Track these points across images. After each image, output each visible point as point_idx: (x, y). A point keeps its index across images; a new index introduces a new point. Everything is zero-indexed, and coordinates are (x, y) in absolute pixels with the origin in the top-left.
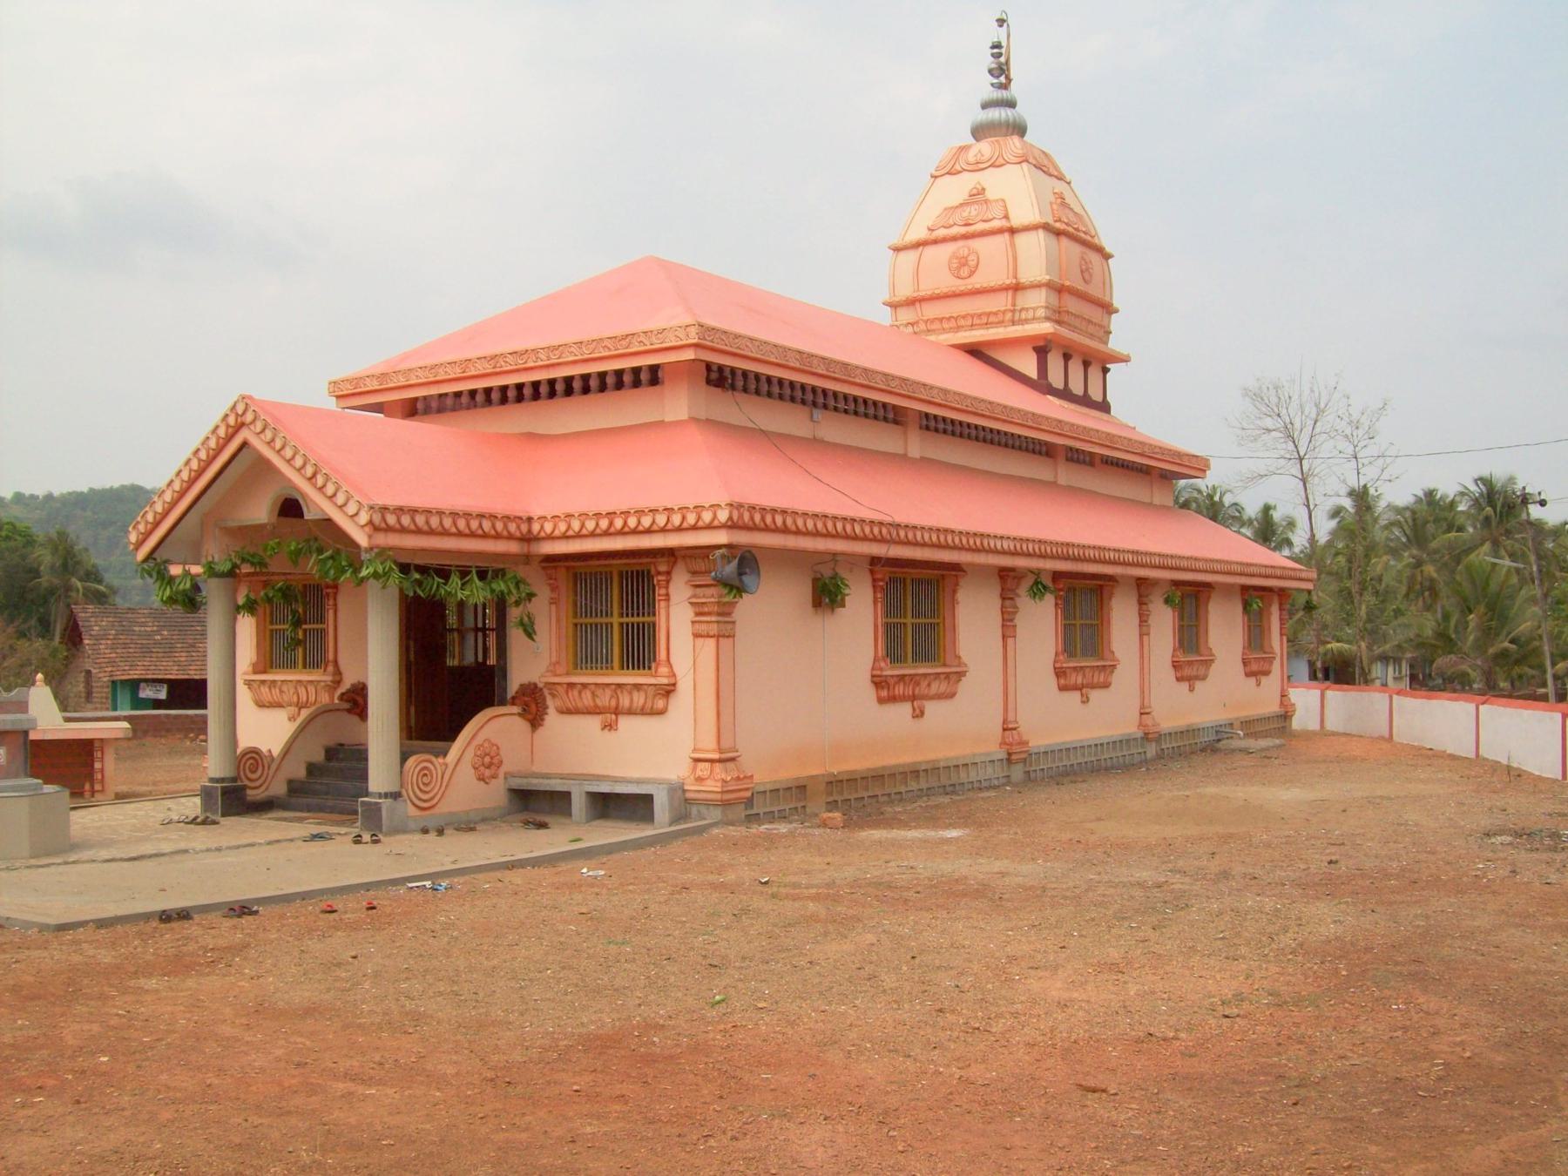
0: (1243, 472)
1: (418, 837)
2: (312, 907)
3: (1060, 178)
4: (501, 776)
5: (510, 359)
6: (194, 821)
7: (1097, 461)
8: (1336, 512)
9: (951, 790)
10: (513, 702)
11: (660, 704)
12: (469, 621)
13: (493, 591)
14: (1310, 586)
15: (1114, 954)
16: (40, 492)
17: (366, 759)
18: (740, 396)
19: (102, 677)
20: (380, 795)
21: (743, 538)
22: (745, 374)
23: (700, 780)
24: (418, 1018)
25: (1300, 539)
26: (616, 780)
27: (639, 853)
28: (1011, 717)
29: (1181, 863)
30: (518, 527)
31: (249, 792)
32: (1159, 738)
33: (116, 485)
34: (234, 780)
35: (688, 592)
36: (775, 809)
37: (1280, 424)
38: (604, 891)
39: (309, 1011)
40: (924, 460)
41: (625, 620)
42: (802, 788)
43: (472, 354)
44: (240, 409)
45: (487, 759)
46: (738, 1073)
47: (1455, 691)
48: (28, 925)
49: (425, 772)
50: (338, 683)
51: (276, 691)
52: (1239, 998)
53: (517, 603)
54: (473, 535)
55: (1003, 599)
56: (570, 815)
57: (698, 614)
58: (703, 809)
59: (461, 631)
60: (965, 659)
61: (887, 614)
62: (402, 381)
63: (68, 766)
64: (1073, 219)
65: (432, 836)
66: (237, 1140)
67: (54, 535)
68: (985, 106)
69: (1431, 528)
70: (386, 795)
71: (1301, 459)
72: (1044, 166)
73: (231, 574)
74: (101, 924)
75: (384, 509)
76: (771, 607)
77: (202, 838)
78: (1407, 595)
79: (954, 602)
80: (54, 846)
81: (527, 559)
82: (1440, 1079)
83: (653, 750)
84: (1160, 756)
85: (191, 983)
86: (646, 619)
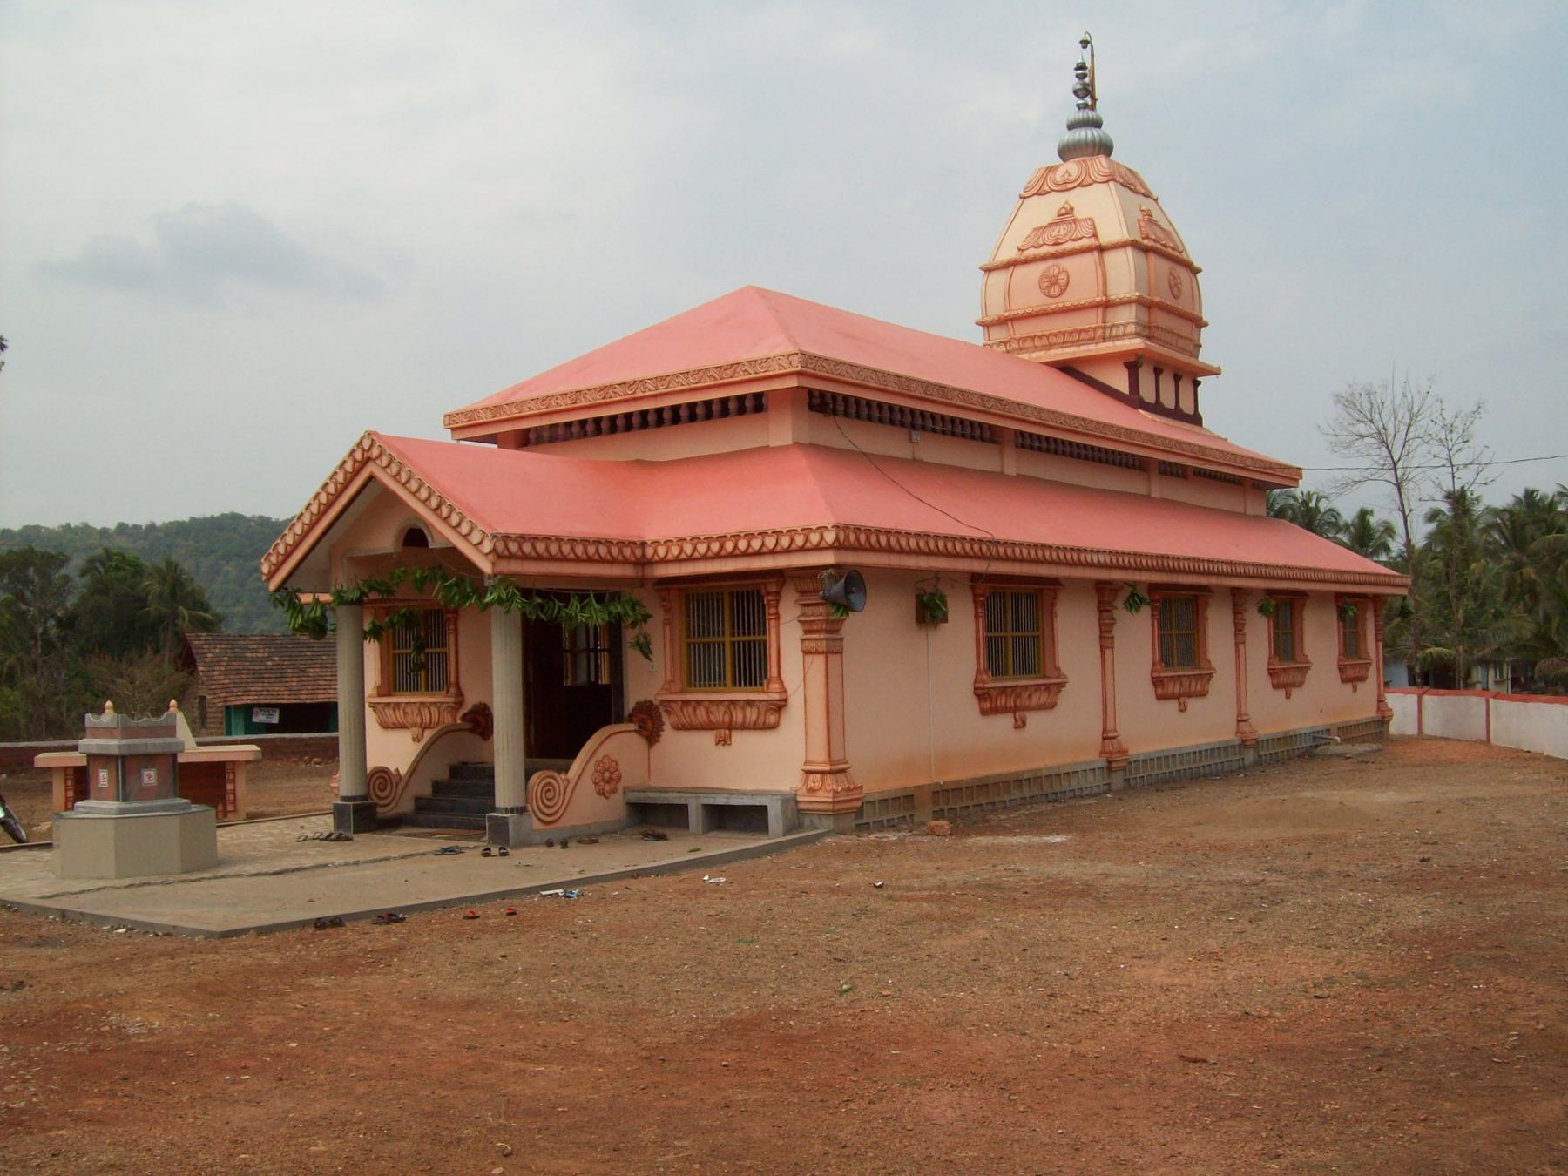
0: (1336, 476)
1: (543, 849)
2: (456, 915)
3: (1147, 195)
4: (620, 789)
5: (619, 390)
6: (328, 838)
7: (1190, 473)
8: (1433, 516)
9: (1053, 798)
10: (630, 719)
11: (772, 719)
12: (582, 643)
13: (610, 613)
14: (1404, 592)
15: (1213, 945)
16: (143, 521)
17: (493, 777)
18: (841, 420)
19: (216, 702)
20: (506, 810)
21: (850, 558)
22: (846, 398)
23: (812, 791)
24: (571, 1008)
25: (1397, 545)
26: (730, 793)
27: (756, 861)
28: (1110, 726)
29: (1278, 862)
30: (633, 552)
31: (379, 810)
32: (1257, 744)
33: (217, 514)
34: (365, 798)
35: (797, 611)
36: (884, 818)
37: (1373, 430)
38: (728, 896)
39: (471, 1004)
40: (1021, 478)
41: (736, 639)
42: (909, 798)
43: (582, 386)
44: (366, 444)
45: (607, 775)
46: (870, 1050)
47: (1556, 694)
48: (195, 932)
49: (548, 788)
50: (460, 703)
51: (400, 714)
52: (1330, 981)
53: (634, 625)
54: (590, 560)
55: (1101, 611)
56: (687, 826)
57: (807, 632)
58: (816, 820)
59: (574, 652)
60: (1064, 671)
61: (988, 628)
62: (515, 413)
63: (205, 784)
64: (1160, 235)
65: (557, 849)
66: (429, 1108)
67: (163, 565)
68: (1072, 126)
69: (1530, 530)
70: (512, 810)
71: (1395, 464)
72: (1130, 183)
73: (359, 602)
74: (262, 931)
75: (506, 538)
76: (876, 626)
77: (338, 854)
78: (1506, 599)
79: (1052, 615)
80: (203, 862)
81: (641, 582)
82: (1514, 1048)
83: (768, 763)
84: (1259, 762)
85: (355, 981)
86: (757, 637)
